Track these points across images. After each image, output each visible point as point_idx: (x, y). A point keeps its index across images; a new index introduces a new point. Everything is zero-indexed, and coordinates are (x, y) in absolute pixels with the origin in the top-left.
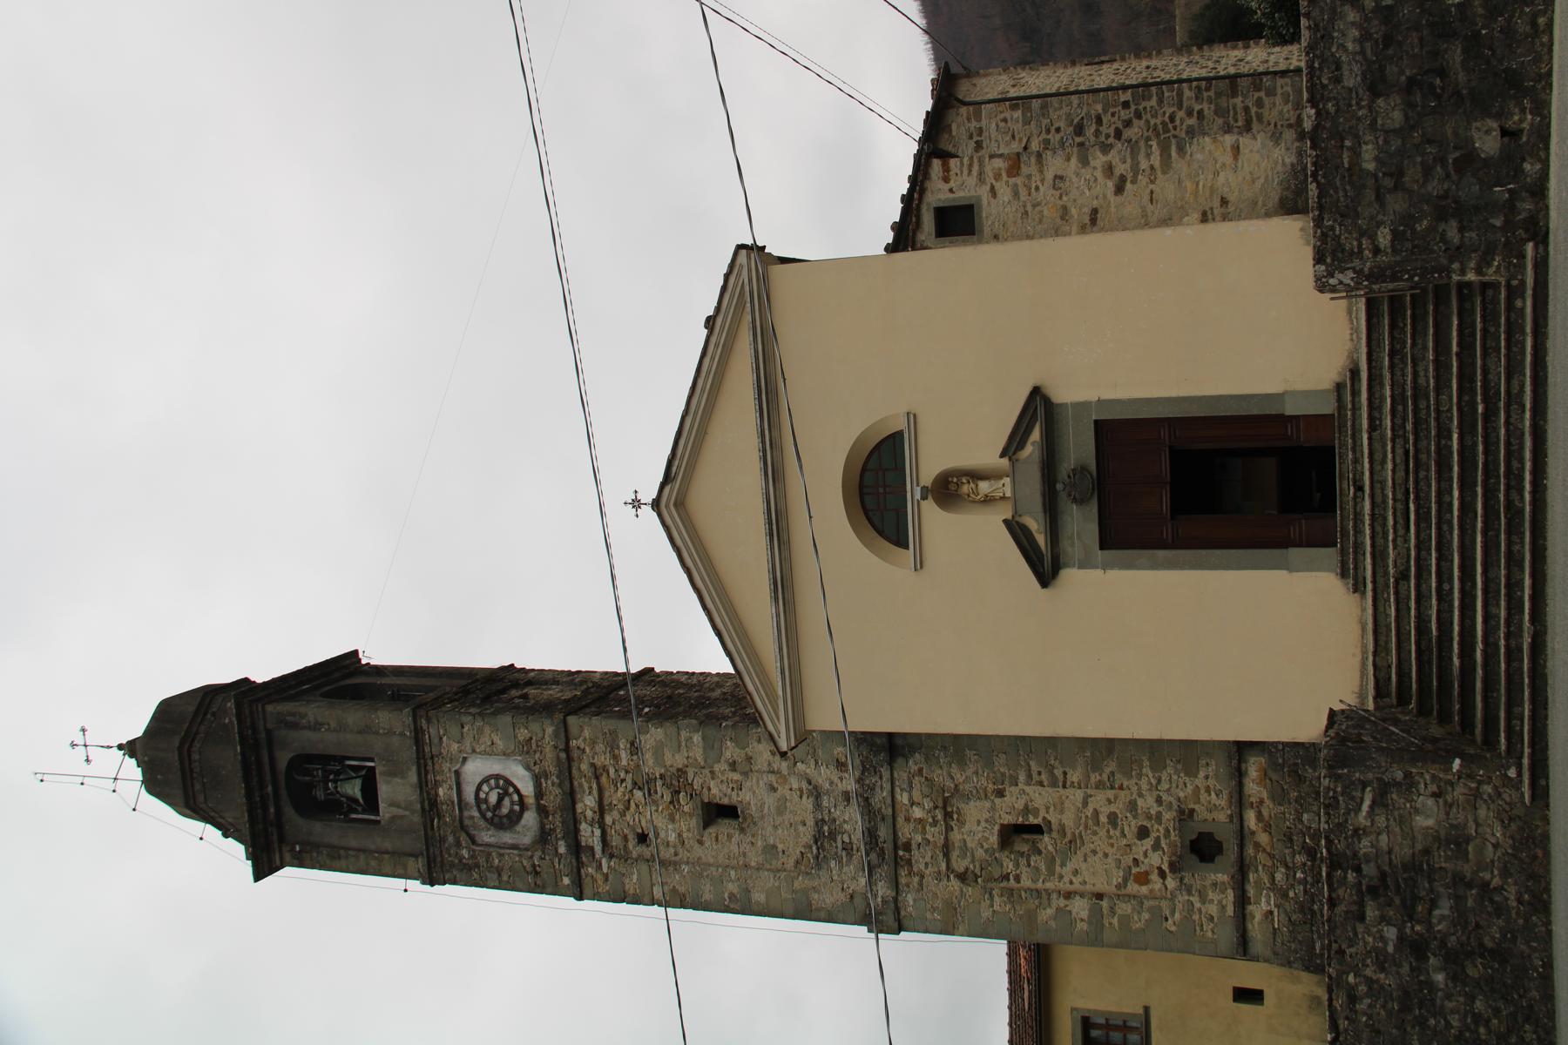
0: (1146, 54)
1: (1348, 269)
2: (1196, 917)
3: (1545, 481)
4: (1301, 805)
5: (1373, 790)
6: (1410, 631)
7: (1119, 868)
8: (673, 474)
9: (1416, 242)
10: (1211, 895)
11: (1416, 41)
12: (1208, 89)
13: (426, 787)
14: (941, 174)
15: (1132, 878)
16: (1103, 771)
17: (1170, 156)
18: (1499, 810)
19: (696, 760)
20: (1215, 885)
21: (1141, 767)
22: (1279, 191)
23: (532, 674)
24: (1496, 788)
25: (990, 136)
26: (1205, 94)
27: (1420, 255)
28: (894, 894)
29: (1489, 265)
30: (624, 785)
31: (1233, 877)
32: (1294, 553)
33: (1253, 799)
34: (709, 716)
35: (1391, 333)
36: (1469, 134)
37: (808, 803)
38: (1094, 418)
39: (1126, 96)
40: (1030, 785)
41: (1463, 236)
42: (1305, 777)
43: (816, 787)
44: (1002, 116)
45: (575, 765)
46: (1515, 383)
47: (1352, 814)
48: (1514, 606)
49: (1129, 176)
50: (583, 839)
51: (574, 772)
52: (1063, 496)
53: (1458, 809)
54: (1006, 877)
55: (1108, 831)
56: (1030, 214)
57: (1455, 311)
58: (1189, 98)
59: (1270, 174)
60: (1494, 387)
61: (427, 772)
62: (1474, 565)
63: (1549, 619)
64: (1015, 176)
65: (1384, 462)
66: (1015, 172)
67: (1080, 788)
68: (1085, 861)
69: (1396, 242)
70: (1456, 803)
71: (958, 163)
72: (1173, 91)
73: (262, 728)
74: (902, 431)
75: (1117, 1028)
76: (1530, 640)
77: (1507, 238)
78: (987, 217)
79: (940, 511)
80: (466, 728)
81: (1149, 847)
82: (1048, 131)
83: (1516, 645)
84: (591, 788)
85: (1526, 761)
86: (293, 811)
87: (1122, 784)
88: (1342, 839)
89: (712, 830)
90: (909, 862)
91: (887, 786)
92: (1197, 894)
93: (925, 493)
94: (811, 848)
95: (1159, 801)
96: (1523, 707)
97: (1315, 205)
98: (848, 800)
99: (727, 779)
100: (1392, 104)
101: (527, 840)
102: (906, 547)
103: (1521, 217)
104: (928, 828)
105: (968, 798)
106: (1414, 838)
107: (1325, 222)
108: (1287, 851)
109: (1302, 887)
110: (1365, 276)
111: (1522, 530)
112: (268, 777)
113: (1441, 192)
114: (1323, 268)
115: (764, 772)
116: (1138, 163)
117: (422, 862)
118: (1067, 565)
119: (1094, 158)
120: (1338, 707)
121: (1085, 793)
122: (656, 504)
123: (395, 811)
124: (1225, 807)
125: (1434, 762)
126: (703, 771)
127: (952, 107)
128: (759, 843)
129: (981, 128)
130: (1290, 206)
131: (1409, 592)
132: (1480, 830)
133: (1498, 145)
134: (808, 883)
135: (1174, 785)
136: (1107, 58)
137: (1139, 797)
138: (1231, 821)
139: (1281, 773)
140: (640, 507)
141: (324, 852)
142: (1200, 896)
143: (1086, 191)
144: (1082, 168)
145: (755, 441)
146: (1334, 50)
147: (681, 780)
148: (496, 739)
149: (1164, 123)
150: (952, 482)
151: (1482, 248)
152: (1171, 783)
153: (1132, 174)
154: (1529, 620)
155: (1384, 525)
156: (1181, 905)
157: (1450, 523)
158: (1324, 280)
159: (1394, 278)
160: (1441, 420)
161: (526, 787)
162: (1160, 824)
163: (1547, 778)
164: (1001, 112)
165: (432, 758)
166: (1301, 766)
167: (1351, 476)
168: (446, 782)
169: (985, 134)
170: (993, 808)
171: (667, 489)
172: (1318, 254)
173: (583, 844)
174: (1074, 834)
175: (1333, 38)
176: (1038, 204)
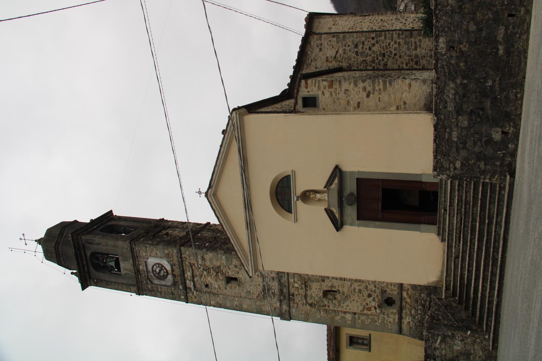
1: (445, 174)
2: (386, 322)
4: (421, 291)
5: (441, 337)
7: (361, 306)
9: (469, 167)
10: (391, 316)
11: (474, 97)
12: (402, 34)
13: (135, 265)
14: (305, 86)
15: (365, 309)
17: (386, 85)
19: (224, 264)
20: (392, 313)
22: (425, 101)
23: (170, 223)
24: (481, 340)
25: (325, 47)
26: (401, 36)
28: (289, 309)
29: (494, 177)
30: (200, 269)
31: (398, 311)
32: (423, 226)
36: (490, 132)
37: (260, 279)
38: (356, 177)
39: (373, 35)
44: (329, 40)
45: (184, 262)
46: (499, 218)
49: (372, 92)
50: (188, 285)
51: (184, 265)
52: (345, 202)
54: (325, 306)
55: (358, 294)
58: (396, 37)
59: (421, 95)
61: (135, 261)
63: (503, 297)
65: (453, 217)
66: (331, 87)
67: (349, 281)
68: (351, 303)
72: (390, 34)
73: (81, 243)
74: (290, 175)
75: (360, 339)
80: (148, 248)
81: (371, 300)
82: (345, 46)
84: (189, 270)
86: (93, 270)
89: (229, 285)
90: (294, 300)
92: (386, 315)
94: (261, 293)
95: (375, 286)
96: (492, 318)
98: (274, 280)
100: (464, 119)
101: (169, 284)
102: (291, 213)
104: (300, 290)
106: (453, 352)
108: (416, 305)
109: (420, 316)
112: (84, 258)
114: (436, 173)
116: (375, 87)
117: (135, 288)
118: (346, 224)
119: (359, 84)
123: (126, 272)
127: (311, 35)
128: (245, 290)
129: (321, 43)
130: (428, 108)
131: (459, 262)
132: (475, 352)
133: (500, 137)
134: (261, 303)
138: (398, 294)
141: (104, 283)
142: (387, 316)
143: (356, 95)
146: (445, 97)
148: (158, 252)
149: (386, 46)
151: (492, 172)
155: (452, 237)
156: (381, 318)
157: (474, 249)
161: (169, 268)
162: (375, 293)
164: (329, 38)
165: (137, 257)
168: (142, 264)
169: (323, 45)
170: (321, 285)
171: (210, 190)
173: (188, 286)
174: (347, 294)
175: (445, 92)
176: (339, 99)
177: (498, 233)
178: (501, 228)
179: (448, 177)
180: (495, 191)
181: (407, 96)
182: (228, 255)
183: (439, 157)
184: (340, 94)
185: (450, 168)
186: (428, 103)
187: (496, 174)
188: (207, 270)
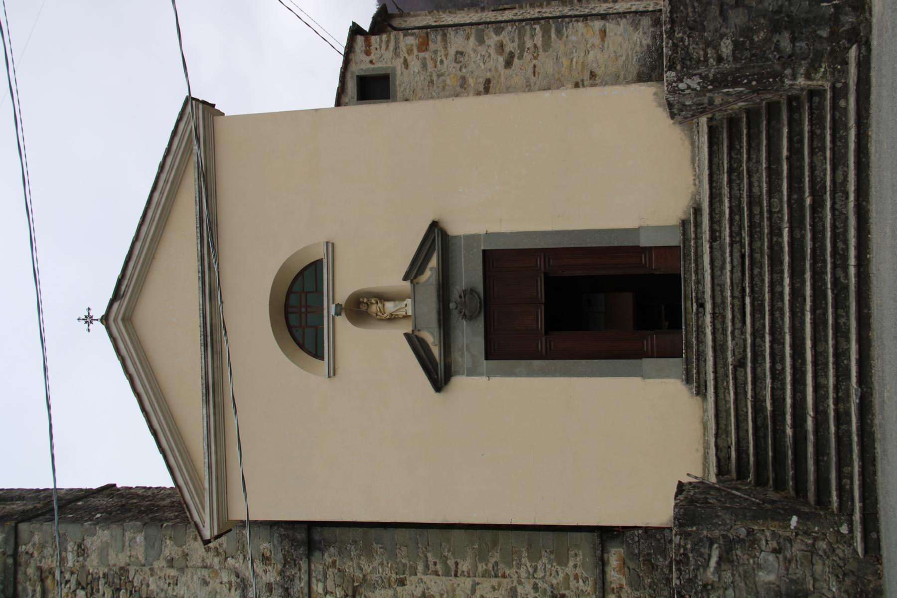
0: (539, 4)
1: (695, 75)
3: (868, 256)
4: (654, 590)
6: (747, 412)
8: (122, 293)
14: (364, 48)
16: (488, 561)
17: (550, 37)
18: (833, 565)
19: (138, 558)
21: (520, 558)
24: (830, 544)
27: (757, 62)
29: (817, 71)
30: (68, 586)
32: (647, 363)
33: (614, 586)
34: (153, 520)
35: (729, 154)
38: (482, 248)
40: (427, 574)
41: (794, 46)
42: (657, 566)
43: (243, 580)
45: (21, 569)
46: (840, 173)
47: (701, 570)
48: (842, 374)
51: (20, 577)
52: (455, 314)
53: (797, 565)
56: (435, 84)
57: (786, 122)
59: (630, 52)
60: (821, 181)
62: (804, 344)
64: (424, 52)
65: (723, 268)
66: (424, 48)
67: (469, 576)
69: (737, 52)
70: (794, 559)
71: (378, 39)
76: (858, 401)
77: (832, 48)
78: (400, 85)
79: (350, 324)
83: (844, 409)
84: (34, 591)
85: (857, 517)
87: (504, 573)
88: (692, 594)
91: (305, 577)
93: (339, 310)
97: (668, 19)
99: (165, 575)
102: (322, 359)
103: (844, 28)
105: (375, 587)
107: (676, 34)
110: (710, 81)
111: (848, 304)
113: (776, 8)
114: (674, 74)
115: (198, 567)
116: (524, 43)
118: (457, 373)
120: (686, 480)
121: (474, 581)
122: (105, 319)
124: (591, 593)
125: (773, 519)
126: (144, 568)
131: (746, 378)
132: (817, 585)
135: (548, 573)
136: (508, 6)
137: (519, 584)
139: (637, 561)
140: (92, 323)
143: (482, 64)
144: (479, 46)
145: (195, 264)
147: (123, 578)
150: (363, 302)
151: (811, 56)
152: (545, 572)
153: (519, 51)
154: (857, 382)
155: (724, 322)
157: (782, 310)
158: (674, 84)
159: (735, 83)
160: (773, 220)
163: (878, 531)
166: (653, 556)
167: (694, 294)
172: (670, 63)
176: (442, 75)
177: (841, 213)
178: (847, 198)
179: (703, 82)
180: (822, 119)
181: (598, 57)
182: (152, 531)
183: (681, 35)
184: (445, 62)
185: (706, 59)
186: (646, 71)
187: (821, 62)
188: (88, 584)
